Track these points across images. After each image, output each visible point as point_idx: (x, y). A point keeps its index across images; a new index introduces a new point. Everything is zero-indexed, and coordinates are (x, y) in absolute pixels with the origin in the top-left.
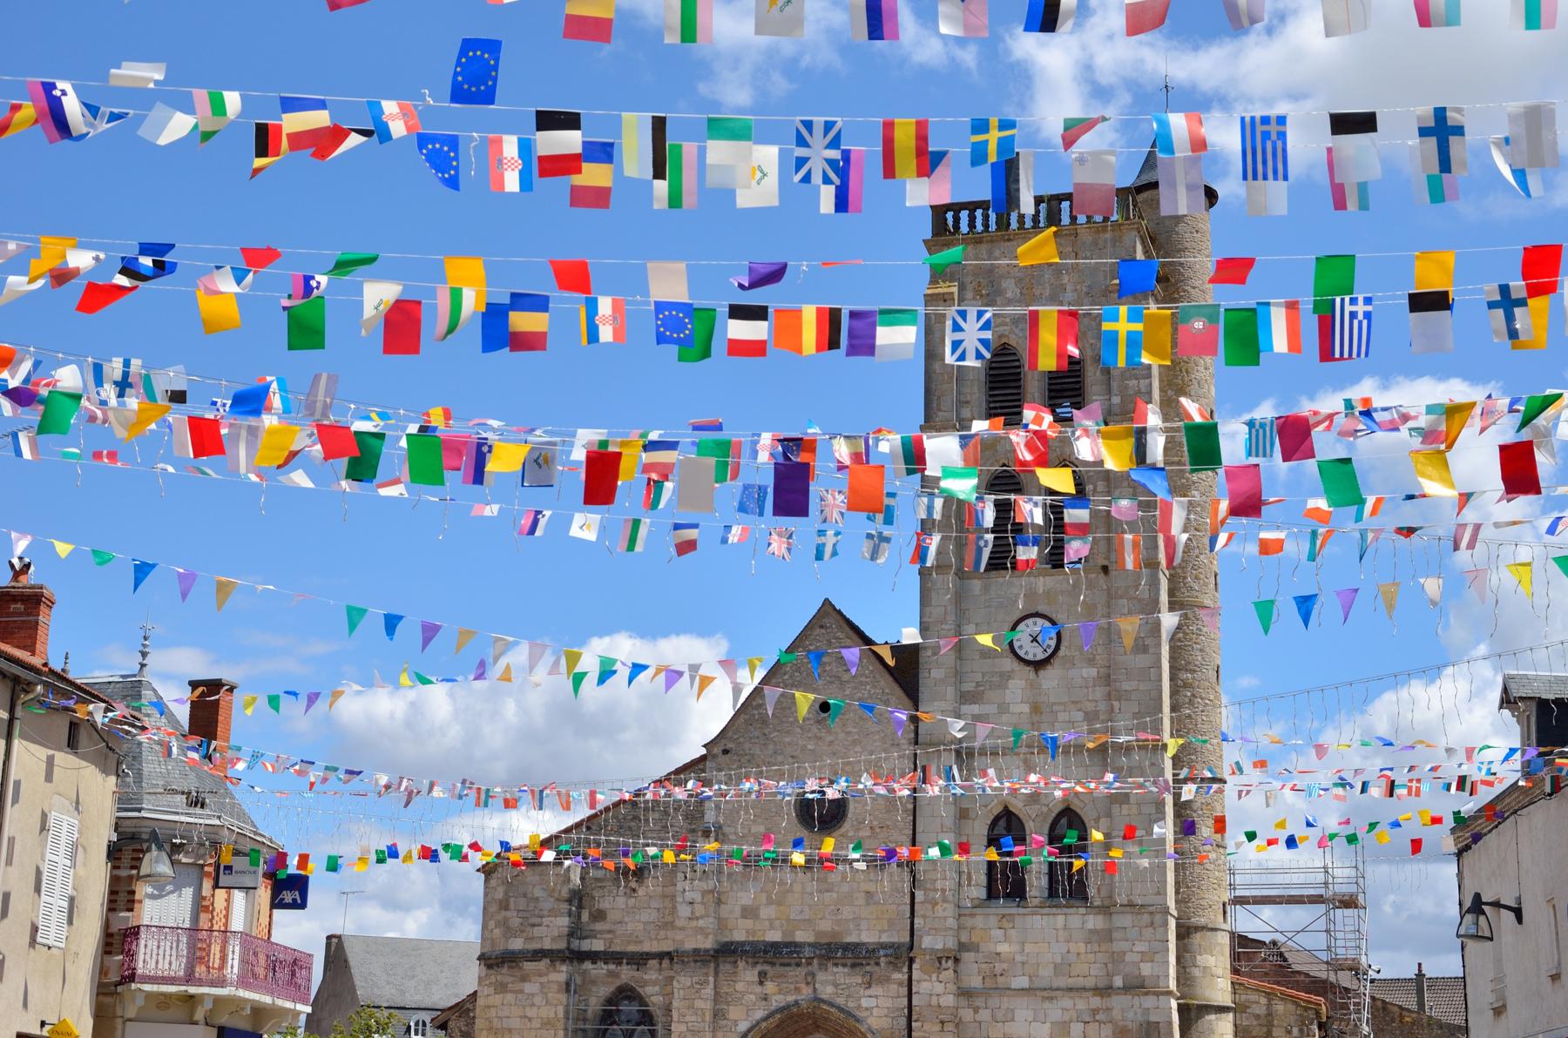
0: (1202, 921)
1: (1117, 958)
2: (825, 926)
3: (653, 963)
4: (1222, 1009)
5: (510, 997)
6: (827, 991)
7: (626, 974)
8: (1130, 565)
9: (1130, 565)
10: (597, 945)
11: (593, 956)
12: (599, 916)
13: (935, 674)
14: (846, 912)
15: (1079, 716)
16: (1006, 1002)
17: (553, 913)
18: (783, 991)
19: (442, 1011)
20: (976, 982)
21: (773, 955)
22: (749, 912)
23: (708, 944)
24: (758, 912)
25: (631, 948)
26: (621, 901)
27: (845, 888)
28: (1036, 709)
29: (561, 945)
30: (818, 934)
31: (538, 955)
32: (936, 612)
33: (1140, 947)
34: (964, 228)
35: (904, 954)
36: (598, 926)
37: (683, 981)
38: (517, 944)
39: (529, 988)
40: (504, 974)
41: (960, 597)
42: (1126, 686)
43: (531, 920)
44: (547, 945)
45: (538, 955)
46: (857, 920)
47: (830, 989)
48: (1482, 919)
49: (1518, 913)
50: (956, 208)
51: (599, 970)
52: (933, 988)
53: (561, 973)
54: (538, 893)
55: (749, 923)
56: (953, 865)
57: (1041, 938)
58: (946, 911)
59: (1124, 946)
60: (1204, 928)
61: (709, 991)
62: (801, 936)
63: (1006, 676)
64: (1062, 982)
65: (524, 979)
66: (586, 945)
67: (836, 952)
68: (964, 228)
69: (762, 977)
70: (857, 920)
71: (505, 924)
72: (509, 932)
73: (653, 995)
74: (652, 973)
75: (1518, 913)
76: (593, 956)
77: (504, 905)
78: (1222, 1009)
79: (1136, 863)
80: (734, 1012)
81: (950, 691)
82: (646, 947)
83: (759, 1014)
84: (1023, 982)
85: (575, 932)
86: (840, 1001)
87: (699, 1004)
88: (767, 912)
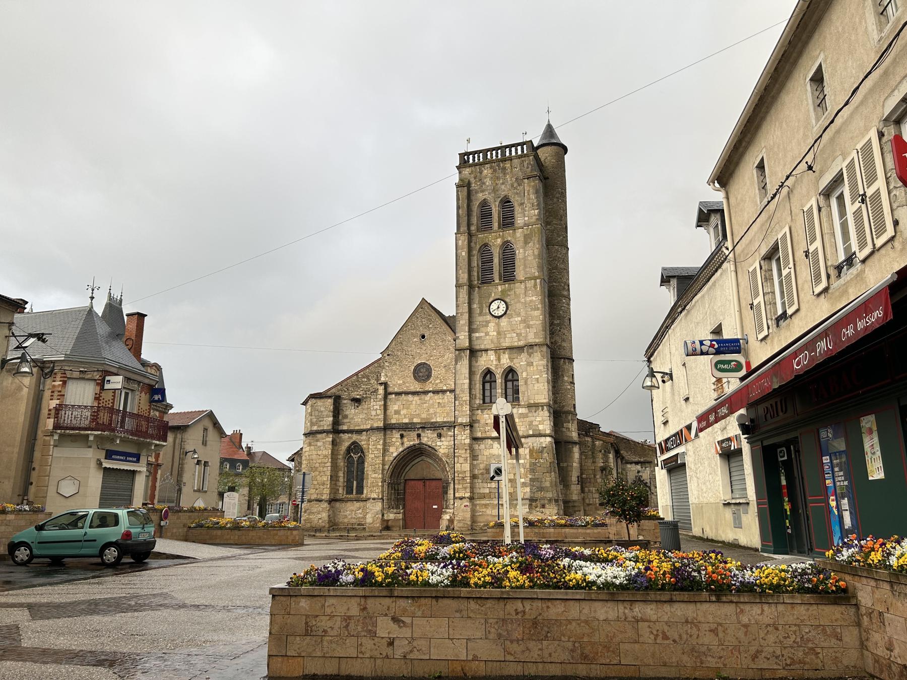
0: (483, 347)
2: (424, 416)
3: (364, 433)
4: (575, 443)
5: (312, 447)
6: (424, 440)
7: (355, 437)
10: (345, 428)
11: (344, 432)
13: (461, 322)
14: (431, 411)
15: (515, 335)
17: (328, 416)
18: (410, 441)
20: (479, 435)
22: (397, 412)
24: (404, 411)
25: (357, 428)
26: (353, 411)
27: (431, 402)
28: (499, 333)
30: (422, 419)
32: (461, 299)
33: (539, 419)
34: (471, 161)
36: (345, 421)
38: (315, 428)
39: (319, 444)
42: (531, 323)
43: (320, 419)
46: (435, 413)
47: (426, 439)
48: (654, 379)
51: (346, 436)
54: (322, 409)
58: (466, 408)
59: (533, 418)
60: (481, 351)
62: (415, 420)
63: (488, 322)
65: (317, 441)
67: (426, 426)
68: (471, 161)
69: (402, 436)
70: (435, 413)
74: (364, 436)
78: (575, 443)
80: (392, 449)
82: (362, 427)
83: (401, 449)
86: (429, 443)
87: (379, 447)
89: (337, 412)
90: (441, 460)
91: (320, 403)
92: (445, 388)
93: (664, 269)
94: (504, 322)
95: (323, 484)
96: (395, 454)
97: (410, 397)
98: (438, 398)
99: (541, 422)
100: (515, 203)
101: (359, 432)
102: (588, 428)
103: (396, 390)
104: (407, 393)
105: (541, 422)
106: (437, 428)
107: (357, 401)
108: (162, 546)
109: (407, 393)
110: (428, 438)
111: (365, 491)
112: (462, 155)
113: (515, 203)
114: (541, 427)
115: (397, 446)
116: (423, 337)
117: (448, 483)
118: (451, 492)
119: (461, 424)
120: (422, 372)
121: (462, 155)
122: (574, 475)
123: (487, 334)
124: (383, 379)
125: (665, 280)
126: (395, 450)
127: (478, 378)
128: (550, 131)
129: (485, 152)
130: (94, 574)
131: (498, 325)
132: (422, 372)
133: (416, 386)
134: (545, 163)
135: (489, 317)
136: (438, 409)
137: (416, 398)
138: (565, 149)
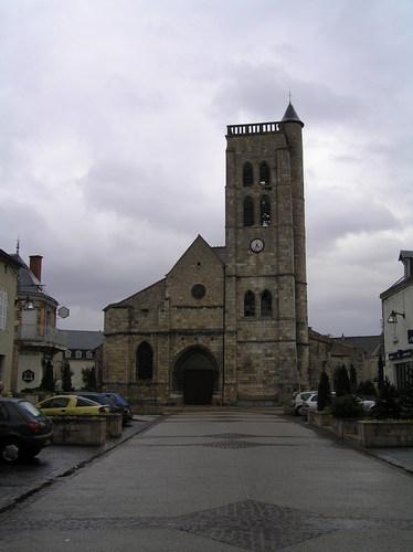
1: (280, 332)
2: (200, 324)
7: (145, 338)
8: (36, 413)
9: (36, 413)
10: (136, 330)
12: (137, 322)
16: (250, 344)
18: (188, 343)
19: (375, 457)
21: (187, 333)
22: (179, 321)
23: (167, 330)
24: (182, 321)
26: (143, 318)
29: (126, 331)
31: (120, 333)
35: (222, 332)
37: (161, 340)
38: (114, 330)
39: (118, 342)
40: (111, 338)
41: (236, 234)
42: (283, 258)
44: (123, 330)
45: (120, 333)
49: (404, 316)
50: (234, 126)
52: (230, 341)
53: (127, 338)
55: (178, 324)
56: (236, 305)
57: (261, 327)
58: (233, 320)
61: (168, 342)
62: (193, 327)
66: (133, 330)
71: (110, 325)
72: (113, 327)
73: (152, 343)
75: (404, 316)
76: (135, 333)
77: (110, 319)
78: (306, 345)
79: (286, 306)
81: (233, 260)
84: (254, 339)
85: (130, 327)
88: (184, 321)
89: (131, 318)
90: (213, 357)
91: (118, 312)
92: (216, 304)
93: (402, 252)
94: (261, 256)
95: (122, 371)
97: (189, 310)
98: (211, 311)
99: (289, 331)
100: (265, 166)
101: (149, 334)
102: (314, 336)
103: (178, 304)
104: (186, 307)
105: (289, 331)
106: (210, 334)
107: (146, 311)
108: (135, 417)
109: (186, 307)
110: (201, 341)
111: (154, 377)
112: (229, 127)
113: (265, 166)
114: (288, 335)
115: (181, 346)
116: (199, 264)
117: (218, 373)
118: (221, 379)
119: (230, 332)
120: (199, 292)
121: (229, 127)
122: (305, 366)
123: (248, 264)
124: (167, 295)
125: (401, 259)
127: (242, 298)
128: (290, 111)
129: (247, 126)
130: (225, 428)
131: (257, 258)
132: (199, 292)
133: (194, 302)
134: (289, 131)
135: (249, 252)
136: (211, 320)
137: (194, 312)
138: (302, 125)
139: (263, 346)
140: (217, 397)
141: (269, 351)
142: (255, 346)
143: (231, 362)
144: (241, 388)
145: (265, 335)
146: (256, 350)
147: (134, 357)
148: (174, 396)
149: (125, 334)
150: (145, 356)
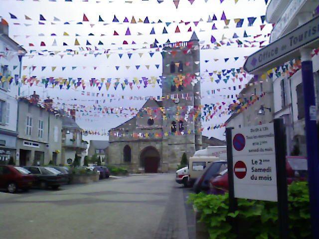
64: (181, 143)
84: (175, 143)
96: (142, 149)
101: (128, 142)
106: (156, 141)
110: (152, 144)
115: (143, 146)
126: (142, 148)
139: (179, 146)
140: (159, 169)
141: (183, 148)
142: (176, 146)
143: (166, 153)
144: (170, 165)
145: (181, 141)
146: (177, 148)
147: (123, 152)
148: (140, 169)
149: (118, 142)
150: (127, 151)
